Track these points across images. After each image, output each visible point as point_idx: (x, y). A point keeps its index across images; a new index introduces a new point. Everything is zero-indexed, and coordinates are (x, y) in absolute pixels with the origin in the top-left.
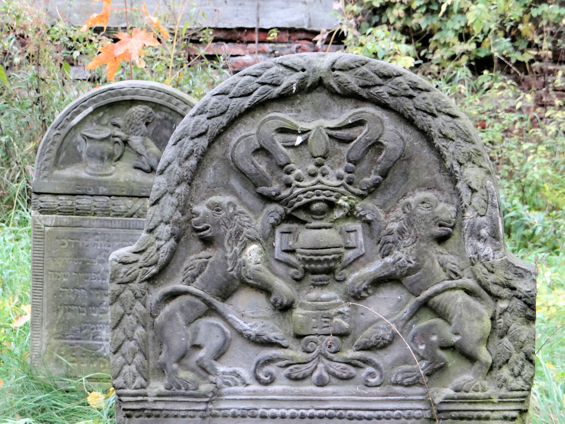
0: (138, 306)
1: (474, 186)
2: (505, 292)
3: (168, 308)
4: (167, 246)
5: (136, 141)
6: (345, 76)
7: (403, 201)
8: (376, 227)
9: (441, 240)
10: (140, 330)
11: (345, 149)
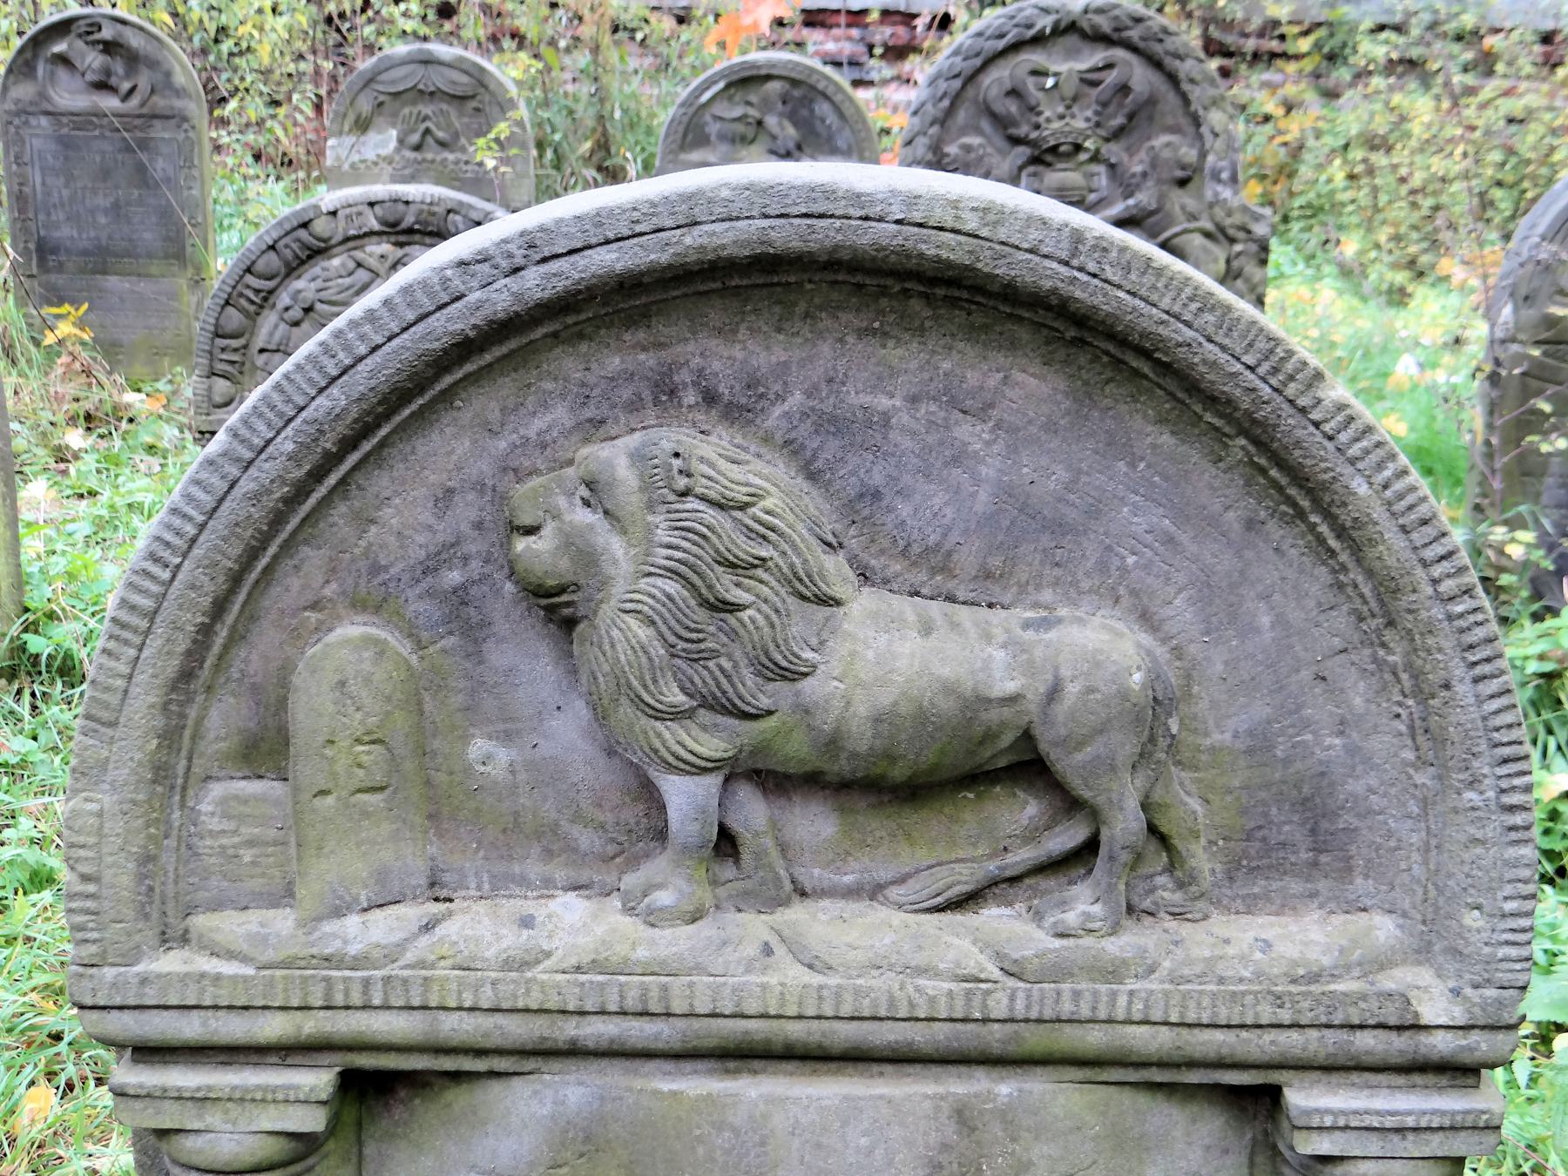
1: (1217, 129)
2: (1241, 235)
5: (771, 121)
8: (1119, 170)
9: (1183, 183)
11: (1094, 92)
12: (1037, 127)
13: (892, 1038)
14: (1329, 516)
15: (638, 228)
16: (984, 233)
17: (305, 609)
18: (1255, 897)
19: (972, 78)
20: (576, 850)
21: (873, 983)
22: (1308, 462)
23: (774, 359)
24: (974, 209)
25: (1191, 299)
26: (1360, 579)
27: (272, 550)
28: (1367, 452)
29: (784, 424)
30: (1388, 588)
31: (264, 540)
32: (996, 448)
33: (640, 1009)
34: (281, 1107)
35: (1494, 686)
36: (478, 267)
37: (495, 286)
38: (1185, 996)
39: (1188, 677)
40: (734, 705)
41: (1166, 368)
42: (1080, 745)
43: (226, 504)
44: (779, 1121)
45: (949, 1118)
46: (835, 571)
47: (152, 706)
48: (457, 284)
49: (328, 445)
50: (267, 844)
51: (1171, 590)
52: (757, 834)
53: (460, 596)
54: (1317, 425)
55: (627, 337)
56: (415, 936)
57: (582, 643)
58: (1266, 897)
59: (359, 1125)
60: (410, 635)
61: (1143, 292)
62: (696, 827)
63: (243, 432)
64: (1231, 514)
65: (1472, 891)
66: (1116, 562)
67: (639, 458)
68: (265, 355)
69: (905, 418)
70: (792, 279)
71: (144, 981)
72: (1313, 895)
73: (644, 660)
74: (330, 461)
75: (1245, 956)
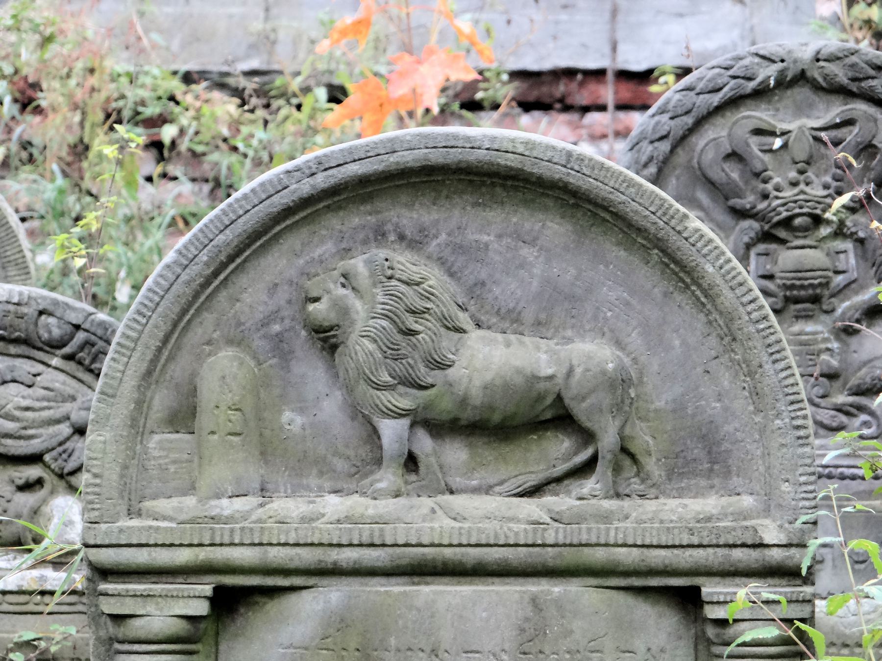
6: (833, 68)
12: (765, 196)
13: (497, 556)
14: (699, 286)
15: (369, 154)
16: (527, 153)
17: (203, 344)
18: (682, 488)
20: (334, 471)
21: (486, 526)
22: (684, 257)
23: (432, 218)
24: (522, 143)
25: (623, 182)
26: (718, 317)
27: (192, 312)
28: (711, 251)
29: (438, 249)
30: (730, 318)
31: (190, 304)
32: (541, 259)
33: (369, 541)
34: (186, 600)
35: (782, 365)
36: (295, 173)
37: (303, 182)
38: (644, 529)
39: (641, 373)
40: (415, 381)
41: (616, 215)
42: (584, 399)
43: (174, 286)
45: (529, 603)
46: (464, 319)
47: (134, 387)
48: (286, 181)
49: (222, 258)
50: (182, 462)
51: (630, 329)
52: (427, 456)
53: (279, 339)
54: (686, 239)
55: (362, 208)
56: (256, 508)
57: (340, 356)
58: (688, 488)
59: (217, 634)
60: (254, 358)
61: (601, 179)
62: (397, 445)
63: (184, 251)
64: (656, 290)
65: (784, 472)
66: (602, 315)
67: (368, 262)
69: (496, 246)
70: (440, 178)
71: (121, 531)
72: (712, 487)
73: (371, 359)
74: (224, 266)
75: (665, 518)
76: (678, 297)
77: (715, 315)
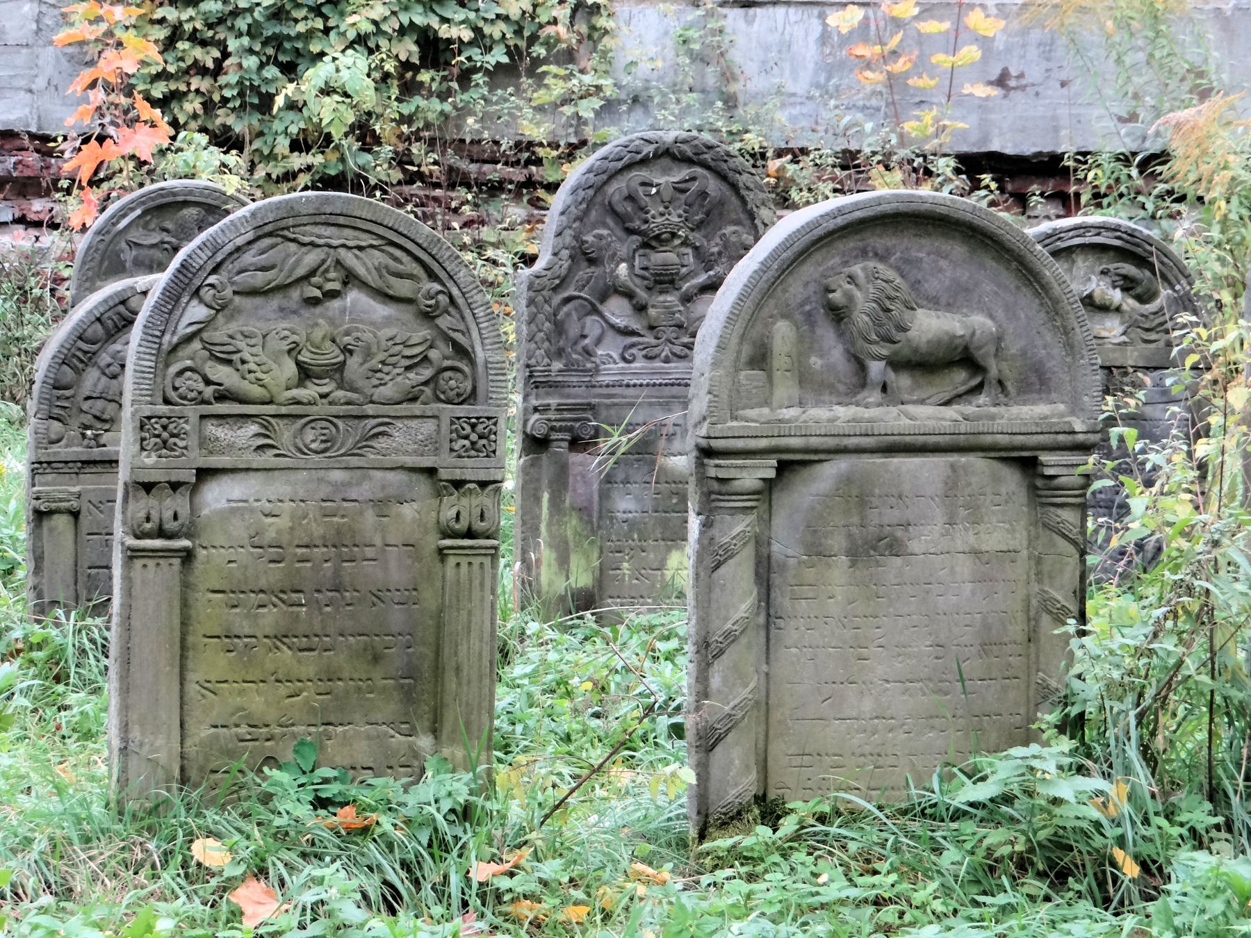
0: (547, 307)
3: (565, 309)
4: (566, 265)
6: (684, 147)
7: (719, 233)
8: (702, 251)
10: (547, 324)
11: (683, 197)
12: (646, 222)
19: (599, 188)
30: (1056, 302)
44: (904, 469)
53: (809, 315)
67: (864, 269)
68: (90, 402)
71: (729, 428)
75: (1022, 416)
76: (1024, 289)
77: (1047, 300)
